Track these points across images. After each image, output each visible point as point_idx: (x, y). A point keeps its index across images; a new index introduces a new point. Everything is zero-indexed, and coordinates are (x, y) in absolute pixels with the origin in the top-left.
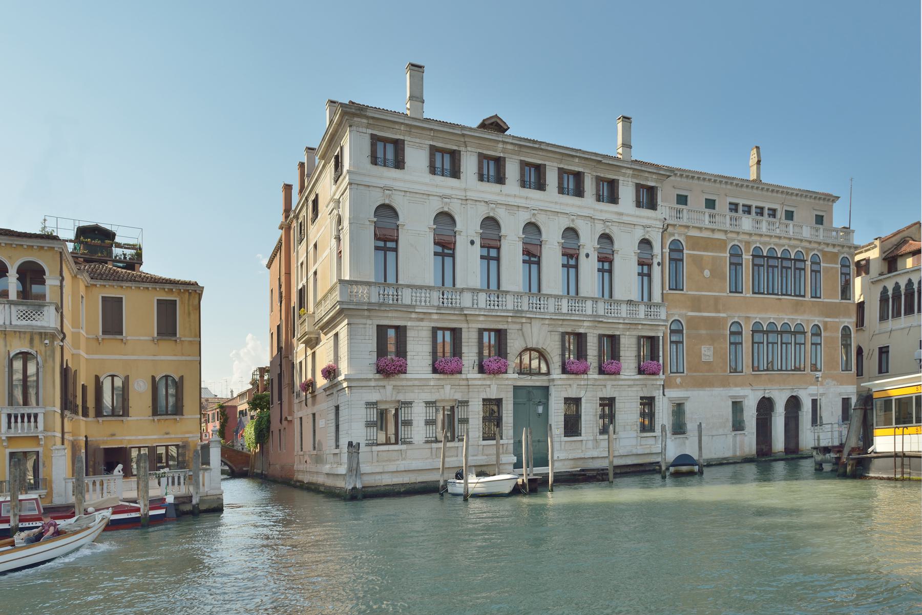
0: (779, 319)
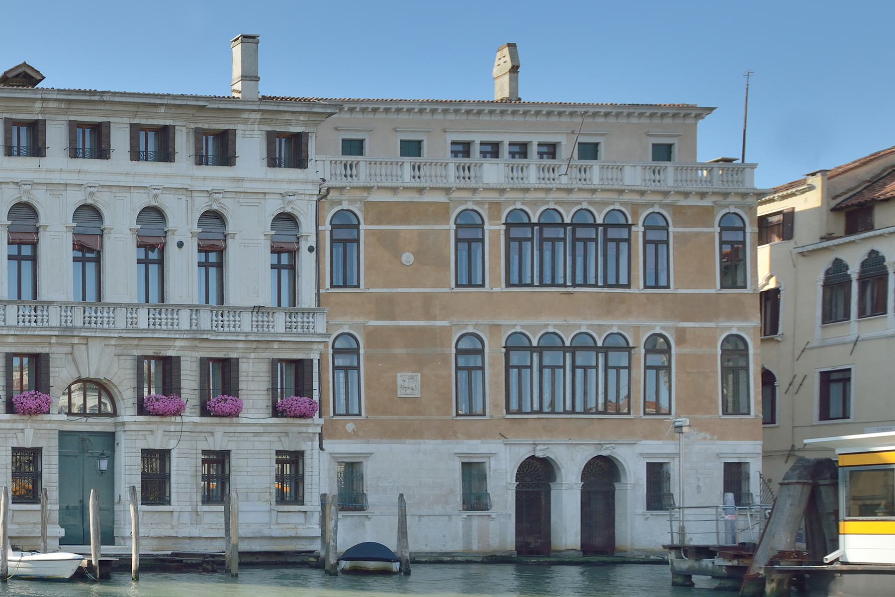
0: (637, 329)
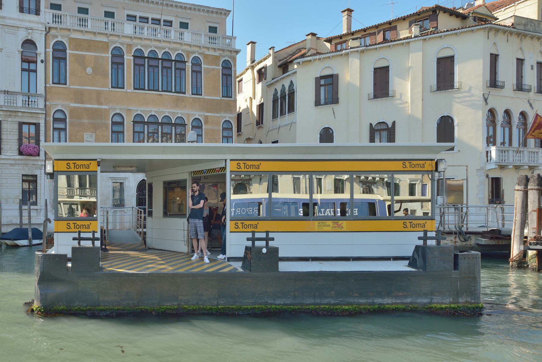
0: (189, 115)
